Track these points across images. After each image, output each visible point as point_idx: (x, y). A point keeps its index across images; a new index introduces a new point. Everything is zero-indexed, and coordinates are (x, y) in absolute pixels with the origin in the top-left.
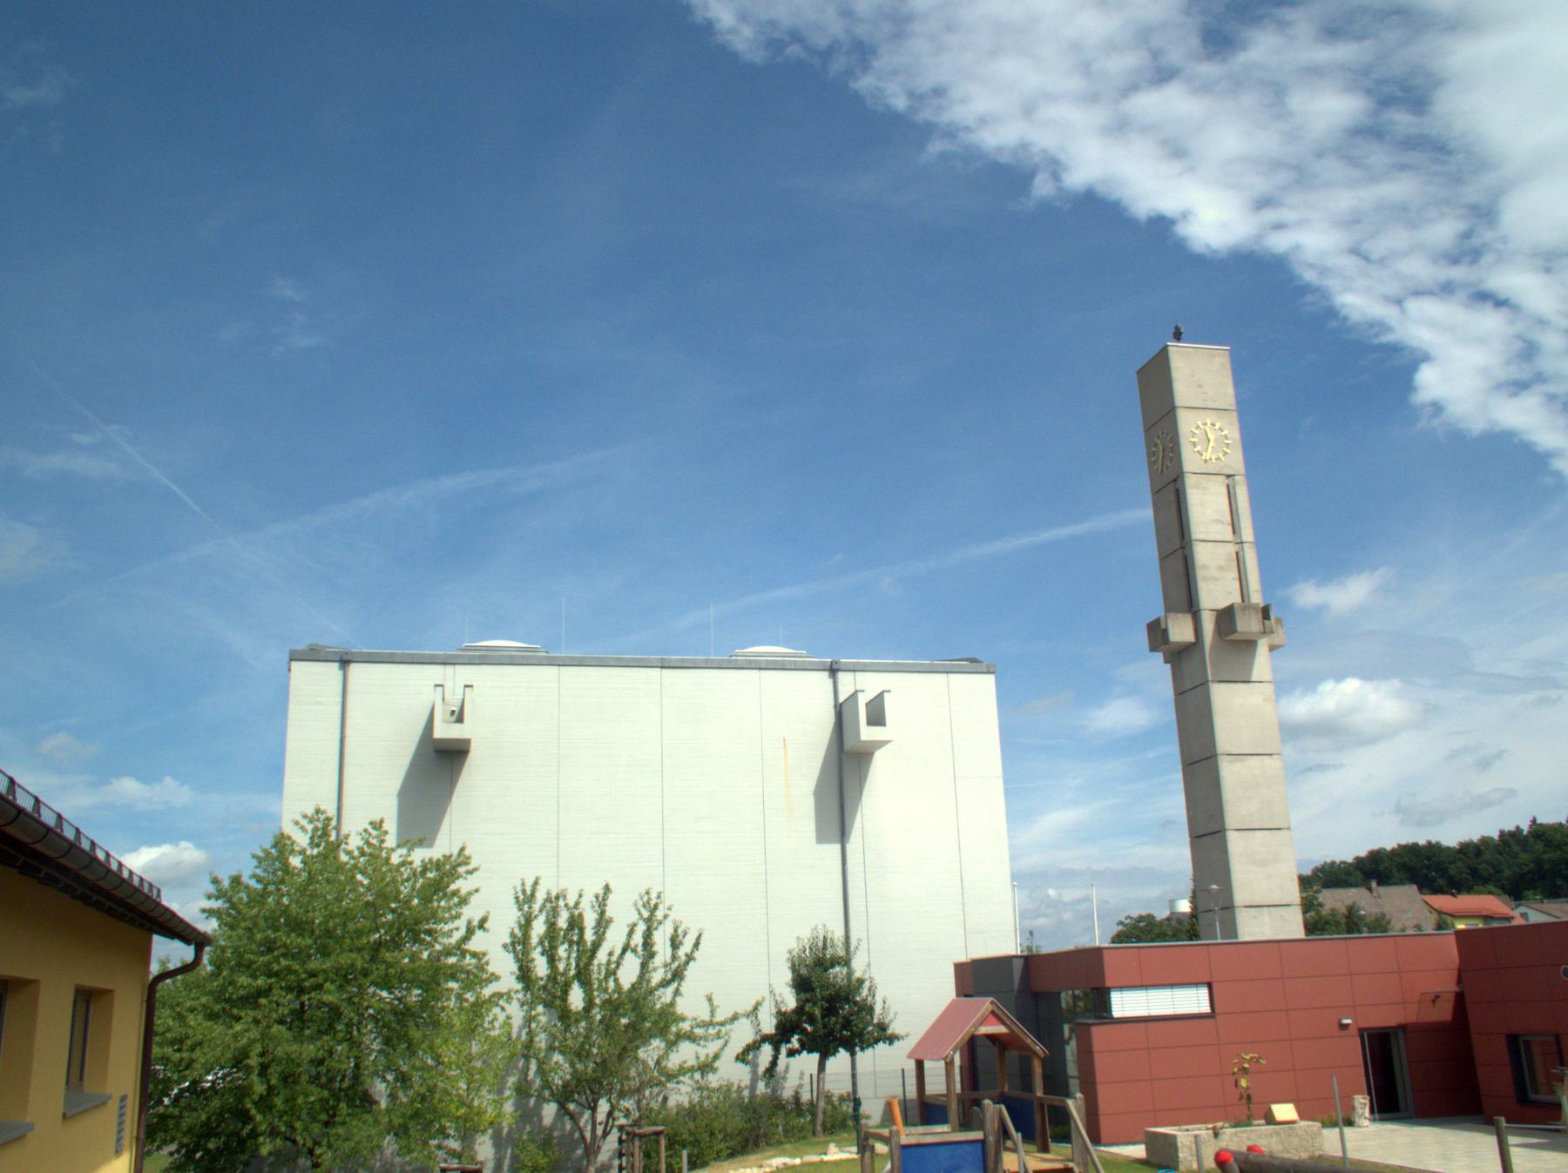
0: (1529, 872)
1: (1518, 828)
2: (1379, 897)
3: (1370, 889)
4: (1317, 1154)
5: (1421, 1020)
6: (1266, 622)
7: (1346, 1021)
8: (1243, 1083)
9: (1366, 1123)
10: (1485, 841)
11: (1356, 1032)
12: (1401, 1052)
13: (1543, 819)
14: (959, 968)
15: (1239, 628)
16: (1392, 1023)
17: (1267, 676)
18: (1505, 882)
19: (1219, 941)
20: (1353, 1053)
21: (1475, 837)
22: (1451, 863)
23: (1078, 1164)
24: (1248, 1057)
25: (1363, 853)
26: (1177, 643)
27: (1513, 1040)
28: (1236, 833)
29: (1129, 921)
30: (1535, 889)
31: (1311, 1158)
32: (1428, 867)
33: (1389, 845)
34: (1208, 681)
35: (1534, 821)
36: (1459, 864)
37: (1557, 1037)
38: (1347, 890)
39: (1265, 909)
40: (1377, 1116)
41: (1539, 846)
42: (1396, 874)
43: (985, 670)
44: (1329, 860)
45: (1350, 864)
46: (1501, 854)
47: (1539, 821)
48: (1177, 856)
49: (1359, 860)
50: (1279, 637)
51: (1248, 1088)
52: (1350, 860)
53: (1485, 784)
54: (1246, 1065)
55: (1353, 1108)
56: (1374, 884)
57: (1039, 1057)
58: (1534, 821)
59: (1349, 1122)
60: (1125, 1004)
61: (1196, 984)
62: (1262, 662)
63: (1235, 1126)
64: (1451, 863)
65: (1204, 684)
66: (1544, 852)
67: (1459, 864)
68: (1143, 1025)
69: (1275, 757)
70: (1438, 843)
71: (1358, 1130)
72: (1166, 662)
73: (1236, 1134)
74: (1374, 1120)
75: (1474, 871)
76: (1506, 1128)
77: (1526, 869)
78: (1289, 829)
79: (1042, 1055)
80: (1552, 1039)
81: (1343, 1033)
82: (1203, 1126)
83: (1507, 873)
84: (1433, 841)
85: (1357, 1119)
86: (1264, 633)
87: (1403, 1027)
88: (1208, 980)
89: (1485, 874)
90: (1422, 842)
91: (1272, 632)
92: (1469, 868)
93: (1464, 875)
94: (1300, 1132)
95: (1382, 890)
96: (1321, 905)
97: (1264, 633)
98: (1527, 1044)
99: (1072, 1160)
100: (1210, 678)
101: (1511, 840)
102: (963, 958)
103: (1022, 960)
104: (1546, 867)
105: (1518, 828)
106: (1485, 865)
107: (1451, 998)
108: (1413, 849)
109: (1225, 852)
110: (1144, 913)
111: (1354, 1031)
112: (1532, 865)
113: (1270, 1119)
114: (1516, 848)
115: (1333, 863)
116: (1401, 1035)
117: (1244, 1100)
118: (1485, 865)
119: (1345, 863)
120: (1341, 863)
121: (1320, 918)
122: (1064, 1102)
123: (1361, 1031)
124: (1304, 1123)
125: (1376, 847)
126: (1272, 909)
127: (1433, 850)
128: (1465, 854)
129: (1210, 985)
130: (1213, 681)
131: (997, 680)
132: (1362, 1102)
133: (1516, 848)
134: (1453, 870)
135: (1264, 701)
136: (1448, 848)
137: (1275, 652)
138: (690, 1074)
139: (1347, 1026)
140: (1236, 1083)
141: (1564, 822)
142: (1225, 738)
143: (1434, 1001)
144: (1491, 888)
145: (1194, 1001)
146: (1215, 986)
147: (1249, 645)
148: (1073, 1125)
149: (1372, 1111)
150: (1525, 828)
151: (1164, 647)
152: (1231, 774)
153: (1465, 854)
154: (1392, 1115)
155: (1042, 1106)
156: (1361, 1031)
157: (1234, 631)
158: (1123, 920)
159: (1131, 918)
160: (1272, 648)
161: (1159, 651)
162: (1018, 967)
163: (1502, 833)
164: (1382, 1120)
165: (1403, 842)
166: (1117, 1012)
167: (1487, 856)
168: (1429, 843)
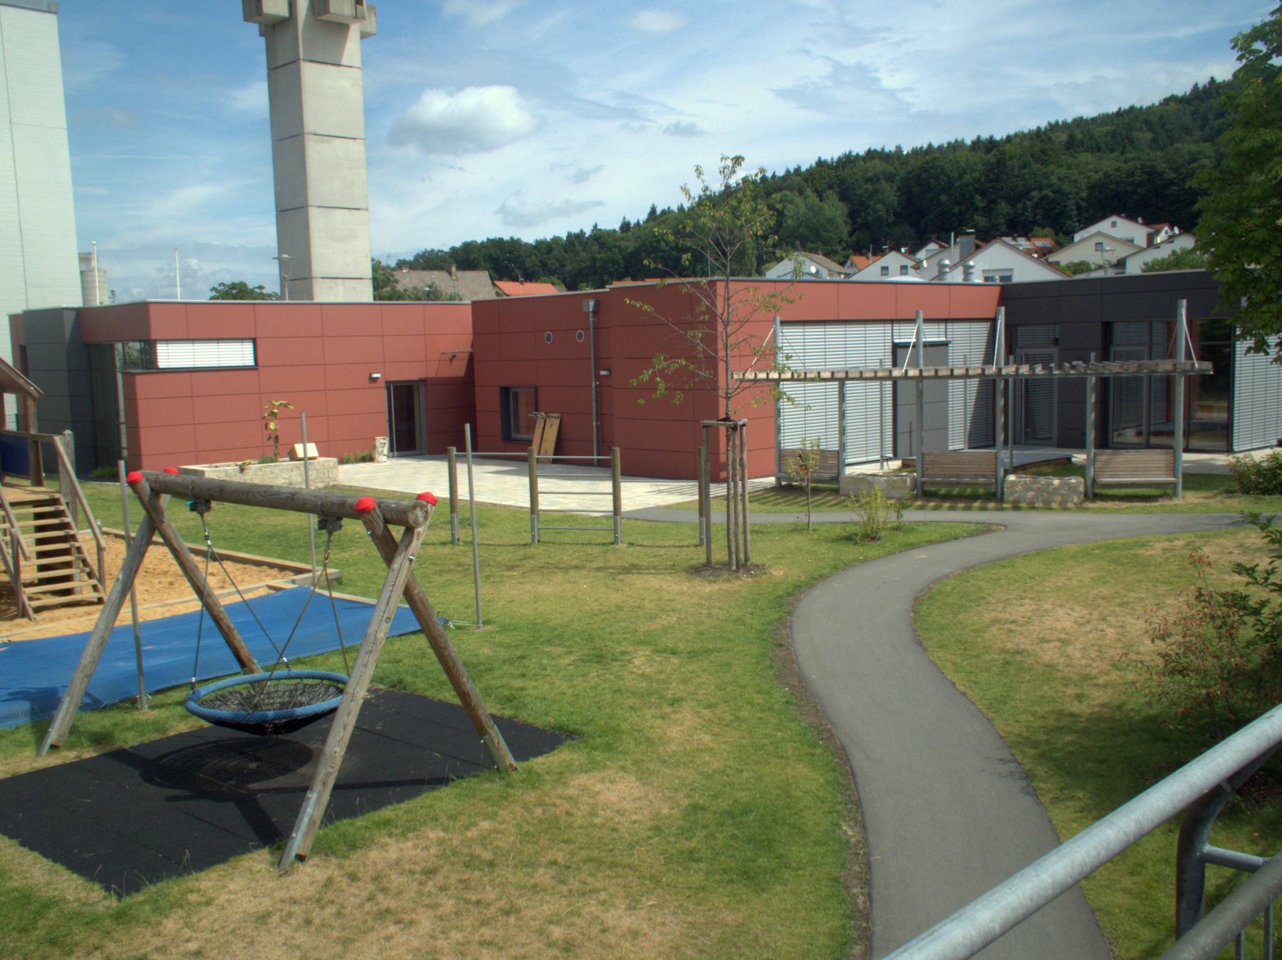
0: (586, 268)
1: (582, 231)
2: (457, 280)
3: (450, 273)
4: (331, 484)
5: (440, 375)
6: (358, 7)
7: (375, 375)
8: (272, 426)
9: (385, 458)
10: (556, 240)
11: (384, 385)
12: (421, 404)
13: (601, 226)
14: (15, 320)
15: (332, 10)
16: (415, 377)
17: (357, 61)
18: (566, 275)
19: (287, 301)
20: (380, 402)
21: (549, 237)
22: (527, 257)
23: (65, 495)
24: (277, 404)
25: (458, 244)
26: (271, 16)
27: (505, 391)
28: (319, 210)
29: (222, 287)
30: (588, 282)
31: (326, 487)
32: (509, 260)
33: (480, 238)
34: (299, 59)
35: (596, 226)
36: (534, 258)
37: (536, 388)
38: (431, 273)
39: (340, 281)
40: (396, 453)
41: (596, 248)
42: (482, 263)
43: (45, 9)
44: (429, 249)
45: (446, 253)
46: (566, 251)
47: (599, 227)
48: (265, 233)
49: (454, 250)
50: (371, 24)
51: (276, 430)
52: (447, 249)
53: (580, 194)
54: (276, 411)
55: (374, 447)
56: (454, 269)
57: (34, 398)
58: (596, 226)
59: (370, 459)
60: (170, 355)
61: (242, 339)
62: (353, 48)
63: (263, 462)
64: (527, 257)
65: (295, 61)
66: (599, 253)
67: (534, 258)
68: (188, 374)
69: (358, 141)
70: (518, 239)
71: (376, 464)
72: (261, 35)
73: (260, 469)
74: (393, 457)
75: (544, 265)
76: (457, 456)
77: (584, 265)
78: (367, 209)
79: (36, 395)
80: (533, 390)
81: (373, 385)
82: (233, 463)
83: (569, 268)
84: (515, 238)
85: (377, 456)
86: (356, 17)
87: (423, 381)
88: (254, 336)
89: (553, 267)
90: (506, 237)
91: (364, 18)
92: (541, 262)
93: (536, 268)
94: (318, 466)
95: (460, 274)
96: (396, 282)
97: (357, 17)
98: (516, 394)
99: (59, 492)
100: (301, 57)
101: (576, 240)
102: (18, 309)
103: (74, 312)
104: (598, 265)
105: (582, 231)
106: (553, 261)
107: (466, 356)
108: (498, 244)
109: (306, 227)
110: (237, 281)
111: (382, 384)
112: (588, 263)
113: (293, 457)
114: (579, 248)
115: (433, 251)
116: (422, 390)
117: (272, 442)
118: (553, 261)
119: (442, 251)
120: (439, 251)
121: (394, 293)
122: (51, 437)
123: (388, 384)
124: (322, 459)
125: (469, 239)
126: (346, 281)
127: (515, 244)
128: (539, 250)
129: (254, 341)
130: (305, 60)
131: (59, 21)
132: (382, 443)
133: (579, 248)
134: (528, 264)
135: (353, 85)
136: (526, 244)
137: (365, 40)
138: (1250, 580)
139: (377, 379)
140: (267, 426)
141: (617, 229)
142: (312, 120)
143: (451, 360)
144: (555, 279)
145: (239, 354)
146: (259, 341)
147: (341, 28)
148: (60, 463)
149: (391, 449)
150: (588, 232)
151: (258, 18)
152: (315, 151)
153: (539, 250)
154: (409, 452)
155: (36, 443)
156: (388, 384)
157: (326, 11)
158: (217, 286)
159: (224, 285)
160: (364, 36)
161: (255, 22)
162: (69, 321)
163: (569, 235)
164: (399, 456)
165: (492, 237)
166: (162, 363)
167: (555, 253)
168: (512, 238)
